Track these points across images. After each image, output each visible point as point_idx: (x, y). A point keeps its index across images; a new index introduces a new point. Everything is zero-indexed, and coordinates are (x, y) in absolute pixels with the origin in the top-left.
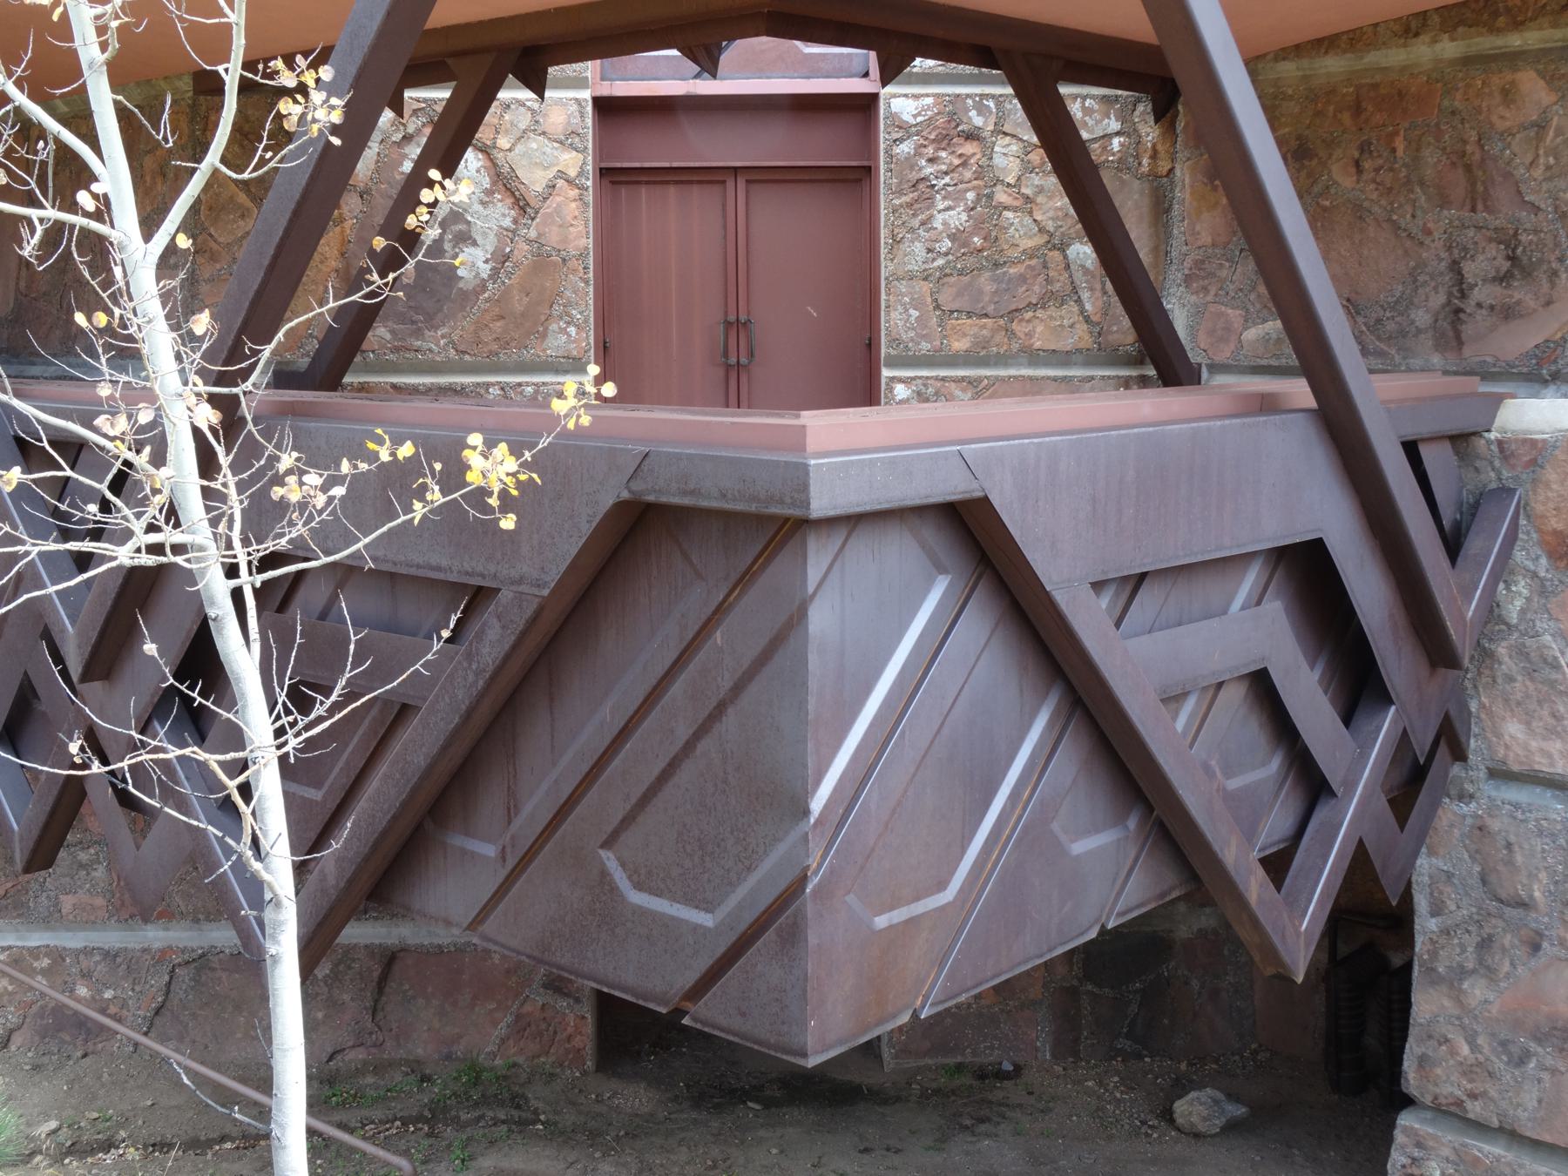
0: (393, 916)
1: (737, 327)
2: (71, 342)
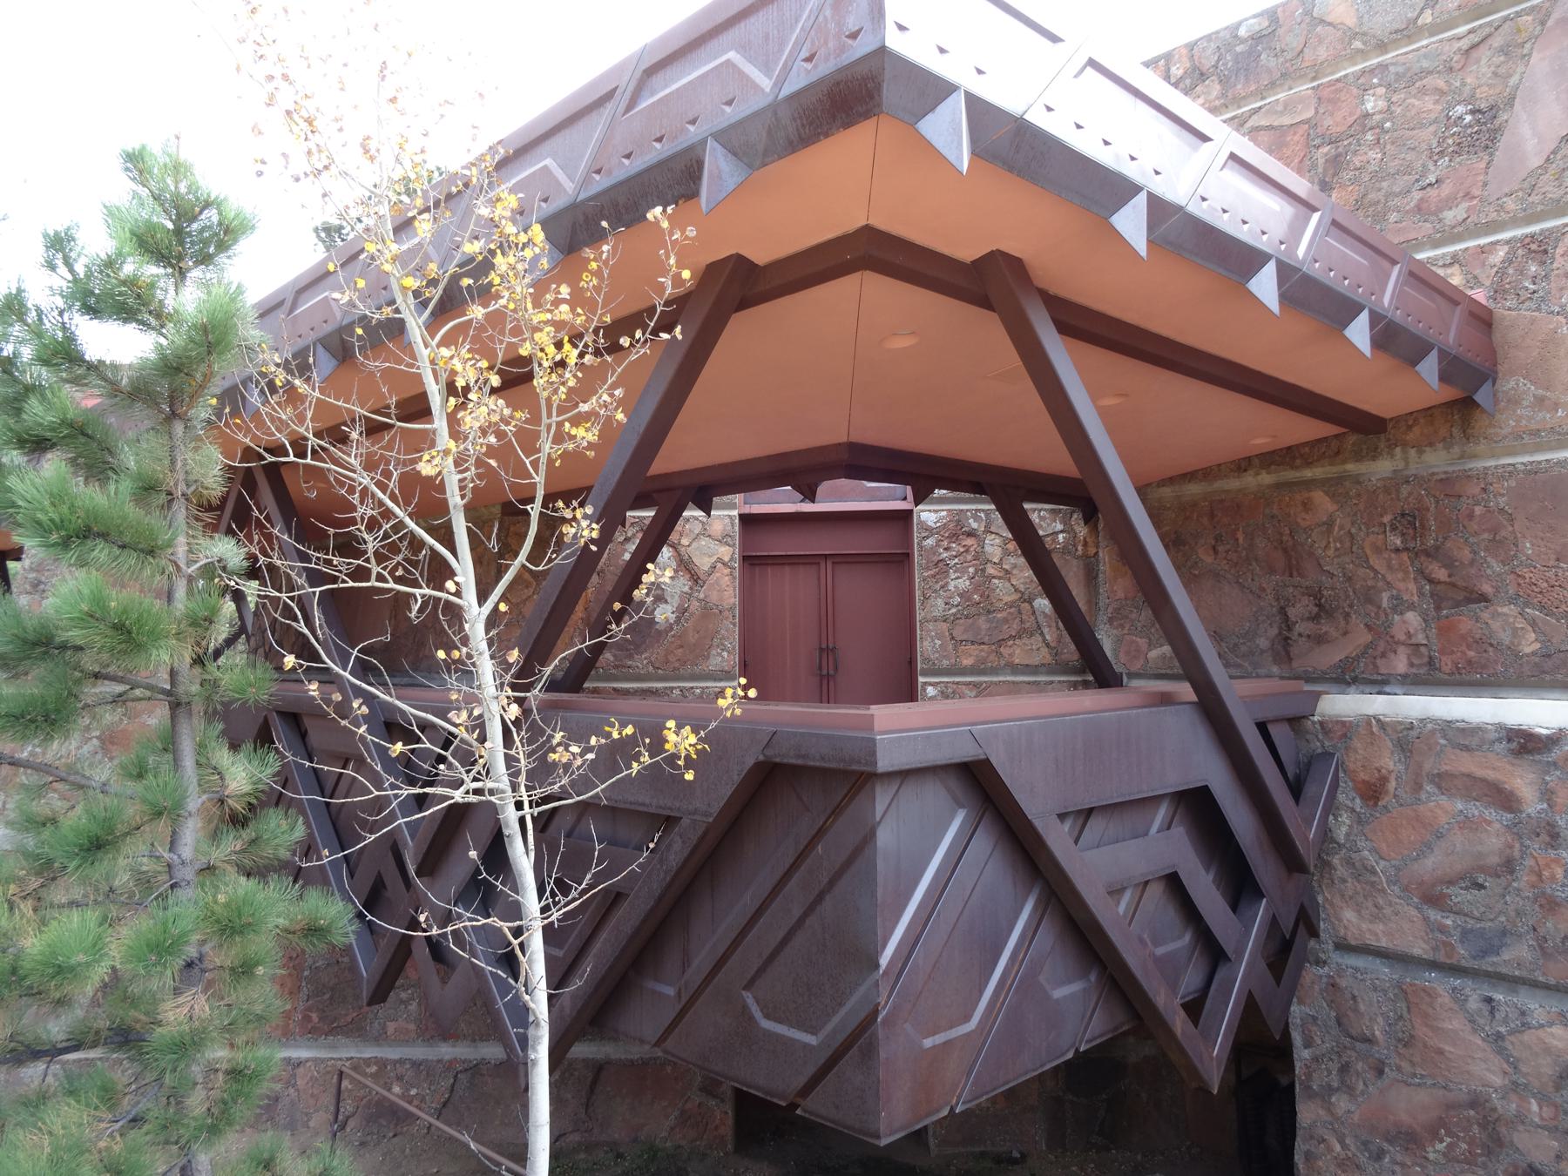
0: (602, 1039)
1: (827, 651)
2: (433, 669)
